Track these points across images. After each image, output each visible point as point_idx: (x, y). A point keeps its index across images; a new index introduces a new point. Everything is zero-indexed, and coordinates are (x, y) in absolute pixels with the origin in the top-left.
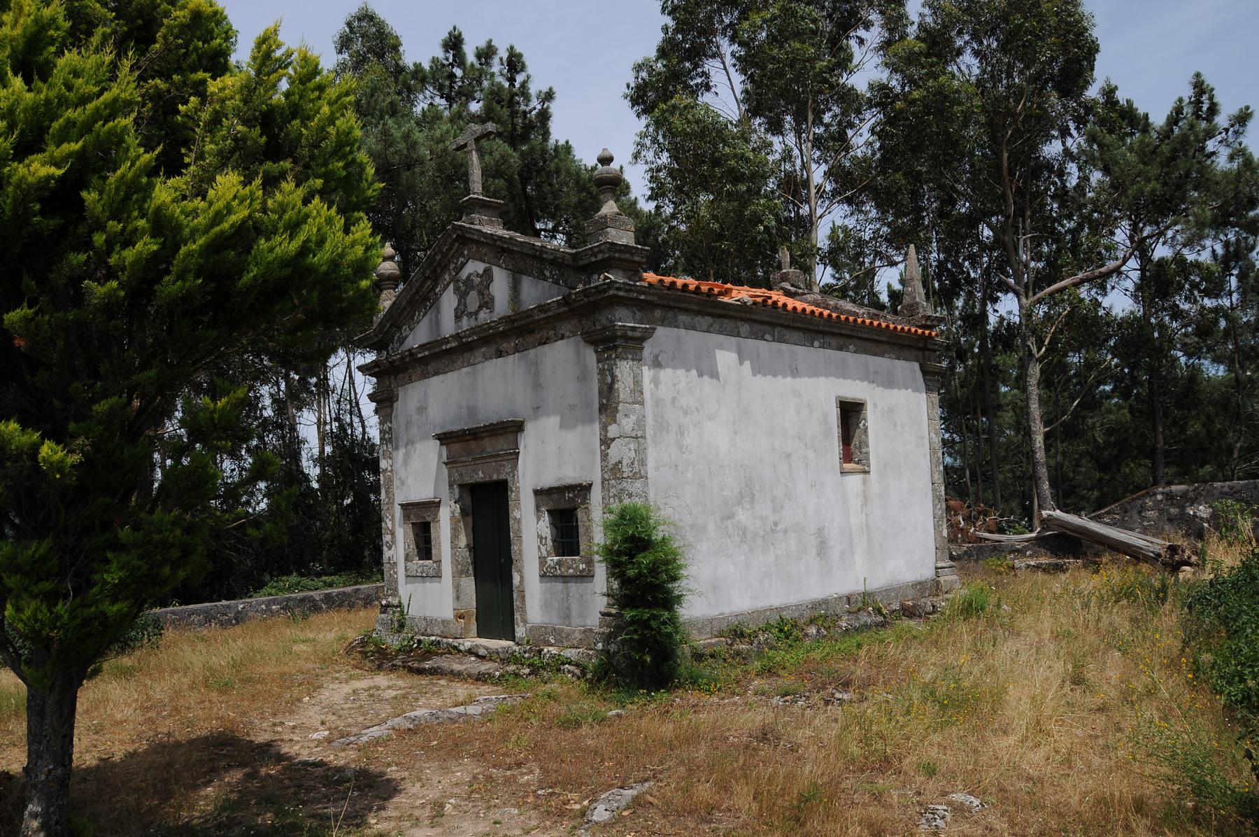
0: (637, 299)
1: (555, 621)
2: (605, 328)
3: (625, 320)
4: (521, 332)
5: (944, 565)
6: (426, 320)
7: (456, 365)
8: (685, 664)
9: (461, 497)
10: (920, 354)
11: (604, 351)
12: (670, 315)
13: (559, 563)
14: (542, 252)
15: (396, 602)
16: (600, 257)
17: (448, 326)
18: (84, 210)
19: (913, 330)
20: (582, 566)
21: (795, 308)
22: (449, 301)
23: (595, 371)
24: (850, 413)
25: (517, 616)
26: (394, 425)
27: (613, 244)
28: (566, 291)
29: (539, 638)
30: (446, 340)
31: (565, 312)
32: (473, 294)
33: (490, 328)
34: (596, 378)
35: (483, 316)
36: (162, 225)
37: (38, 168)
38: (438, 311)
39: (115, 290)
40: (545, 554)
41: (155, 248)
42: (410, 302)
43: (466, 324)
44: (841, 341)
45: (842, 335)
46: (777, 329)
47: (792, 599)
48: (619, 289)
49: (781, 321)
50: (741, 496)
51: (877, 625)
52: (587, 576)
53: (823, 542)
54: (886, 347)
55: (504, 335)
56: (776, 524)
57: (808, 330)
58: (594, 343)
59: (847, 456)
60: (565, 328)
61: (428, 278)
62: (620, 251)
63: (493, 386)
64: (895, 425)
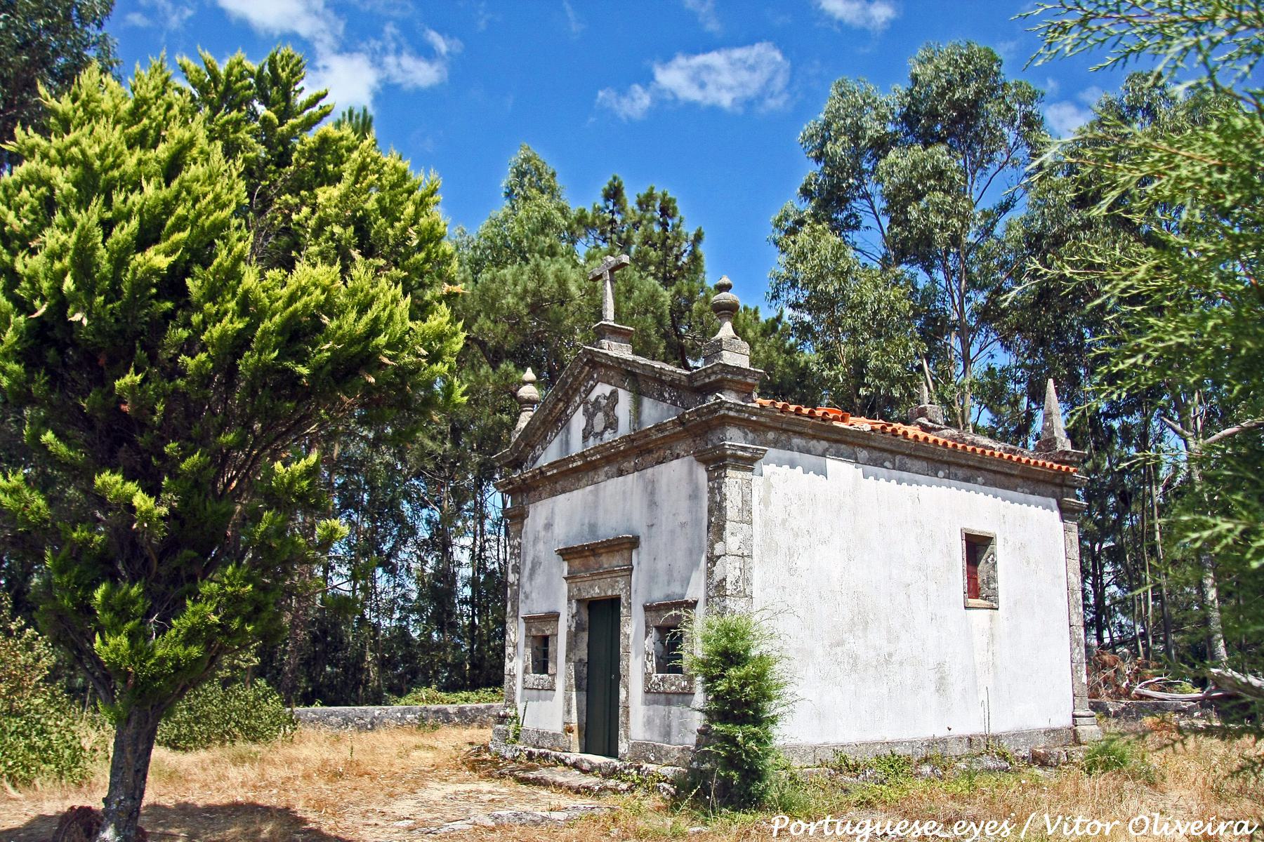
0: (748, 420)
1: (656, 739)
2: (715, 447)
3: (734, 439)
4: (641, 450)
5: (1082, 713)
6: (557, 440)
7: (582, 484)
8: (774, 784)
9: (578, 612)
10: (1058, 490)
11: (715, 470)
12: (783, 437)
13: (663, 680)
14: (661, 374)
15: (512, 714)
16: (713, 378)
17: (577, 446)
18: (188, 296)
19: (1048, 464)
20: (684, 683)
21: (916, 437)
22: (578, 421)
23: (706, 489)
24: (977, 546)
25: (621, 732)
26: (524, 541)
27: (725, 365)
28: (681, 411)
29: (642, 752)
30: (572, 459)
31: (680, 432)
32: (600, 415)
33: (612, 447)
34: (705, 496)
35: (608, 436)
36: (246, 305)
37: (157, 259)
38: (568, 431)
39: (204, 363)
40: (650, 670)
41: (241, 326)
42: (543, 422)
43: (592, 443)
44: (969, 473)
45: (969, 466)
46: (898, 458)
47: (906, 735)
48: (729, 409)
49: (902, 450)
50: (853, 623)
51: (1001, 769)
52: (687, 694)
53: (942, 678)
54: (1019, 481)
55: (625, 455)
56: (890, 655)
57: (933, 460)
58: (705, 462)
59: (973, 590)
60: (680, 448)
61: (560, 400)
62: (733, 373)
63: (613, 503)
64: (1028, 563)
